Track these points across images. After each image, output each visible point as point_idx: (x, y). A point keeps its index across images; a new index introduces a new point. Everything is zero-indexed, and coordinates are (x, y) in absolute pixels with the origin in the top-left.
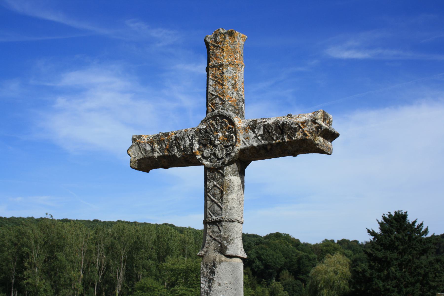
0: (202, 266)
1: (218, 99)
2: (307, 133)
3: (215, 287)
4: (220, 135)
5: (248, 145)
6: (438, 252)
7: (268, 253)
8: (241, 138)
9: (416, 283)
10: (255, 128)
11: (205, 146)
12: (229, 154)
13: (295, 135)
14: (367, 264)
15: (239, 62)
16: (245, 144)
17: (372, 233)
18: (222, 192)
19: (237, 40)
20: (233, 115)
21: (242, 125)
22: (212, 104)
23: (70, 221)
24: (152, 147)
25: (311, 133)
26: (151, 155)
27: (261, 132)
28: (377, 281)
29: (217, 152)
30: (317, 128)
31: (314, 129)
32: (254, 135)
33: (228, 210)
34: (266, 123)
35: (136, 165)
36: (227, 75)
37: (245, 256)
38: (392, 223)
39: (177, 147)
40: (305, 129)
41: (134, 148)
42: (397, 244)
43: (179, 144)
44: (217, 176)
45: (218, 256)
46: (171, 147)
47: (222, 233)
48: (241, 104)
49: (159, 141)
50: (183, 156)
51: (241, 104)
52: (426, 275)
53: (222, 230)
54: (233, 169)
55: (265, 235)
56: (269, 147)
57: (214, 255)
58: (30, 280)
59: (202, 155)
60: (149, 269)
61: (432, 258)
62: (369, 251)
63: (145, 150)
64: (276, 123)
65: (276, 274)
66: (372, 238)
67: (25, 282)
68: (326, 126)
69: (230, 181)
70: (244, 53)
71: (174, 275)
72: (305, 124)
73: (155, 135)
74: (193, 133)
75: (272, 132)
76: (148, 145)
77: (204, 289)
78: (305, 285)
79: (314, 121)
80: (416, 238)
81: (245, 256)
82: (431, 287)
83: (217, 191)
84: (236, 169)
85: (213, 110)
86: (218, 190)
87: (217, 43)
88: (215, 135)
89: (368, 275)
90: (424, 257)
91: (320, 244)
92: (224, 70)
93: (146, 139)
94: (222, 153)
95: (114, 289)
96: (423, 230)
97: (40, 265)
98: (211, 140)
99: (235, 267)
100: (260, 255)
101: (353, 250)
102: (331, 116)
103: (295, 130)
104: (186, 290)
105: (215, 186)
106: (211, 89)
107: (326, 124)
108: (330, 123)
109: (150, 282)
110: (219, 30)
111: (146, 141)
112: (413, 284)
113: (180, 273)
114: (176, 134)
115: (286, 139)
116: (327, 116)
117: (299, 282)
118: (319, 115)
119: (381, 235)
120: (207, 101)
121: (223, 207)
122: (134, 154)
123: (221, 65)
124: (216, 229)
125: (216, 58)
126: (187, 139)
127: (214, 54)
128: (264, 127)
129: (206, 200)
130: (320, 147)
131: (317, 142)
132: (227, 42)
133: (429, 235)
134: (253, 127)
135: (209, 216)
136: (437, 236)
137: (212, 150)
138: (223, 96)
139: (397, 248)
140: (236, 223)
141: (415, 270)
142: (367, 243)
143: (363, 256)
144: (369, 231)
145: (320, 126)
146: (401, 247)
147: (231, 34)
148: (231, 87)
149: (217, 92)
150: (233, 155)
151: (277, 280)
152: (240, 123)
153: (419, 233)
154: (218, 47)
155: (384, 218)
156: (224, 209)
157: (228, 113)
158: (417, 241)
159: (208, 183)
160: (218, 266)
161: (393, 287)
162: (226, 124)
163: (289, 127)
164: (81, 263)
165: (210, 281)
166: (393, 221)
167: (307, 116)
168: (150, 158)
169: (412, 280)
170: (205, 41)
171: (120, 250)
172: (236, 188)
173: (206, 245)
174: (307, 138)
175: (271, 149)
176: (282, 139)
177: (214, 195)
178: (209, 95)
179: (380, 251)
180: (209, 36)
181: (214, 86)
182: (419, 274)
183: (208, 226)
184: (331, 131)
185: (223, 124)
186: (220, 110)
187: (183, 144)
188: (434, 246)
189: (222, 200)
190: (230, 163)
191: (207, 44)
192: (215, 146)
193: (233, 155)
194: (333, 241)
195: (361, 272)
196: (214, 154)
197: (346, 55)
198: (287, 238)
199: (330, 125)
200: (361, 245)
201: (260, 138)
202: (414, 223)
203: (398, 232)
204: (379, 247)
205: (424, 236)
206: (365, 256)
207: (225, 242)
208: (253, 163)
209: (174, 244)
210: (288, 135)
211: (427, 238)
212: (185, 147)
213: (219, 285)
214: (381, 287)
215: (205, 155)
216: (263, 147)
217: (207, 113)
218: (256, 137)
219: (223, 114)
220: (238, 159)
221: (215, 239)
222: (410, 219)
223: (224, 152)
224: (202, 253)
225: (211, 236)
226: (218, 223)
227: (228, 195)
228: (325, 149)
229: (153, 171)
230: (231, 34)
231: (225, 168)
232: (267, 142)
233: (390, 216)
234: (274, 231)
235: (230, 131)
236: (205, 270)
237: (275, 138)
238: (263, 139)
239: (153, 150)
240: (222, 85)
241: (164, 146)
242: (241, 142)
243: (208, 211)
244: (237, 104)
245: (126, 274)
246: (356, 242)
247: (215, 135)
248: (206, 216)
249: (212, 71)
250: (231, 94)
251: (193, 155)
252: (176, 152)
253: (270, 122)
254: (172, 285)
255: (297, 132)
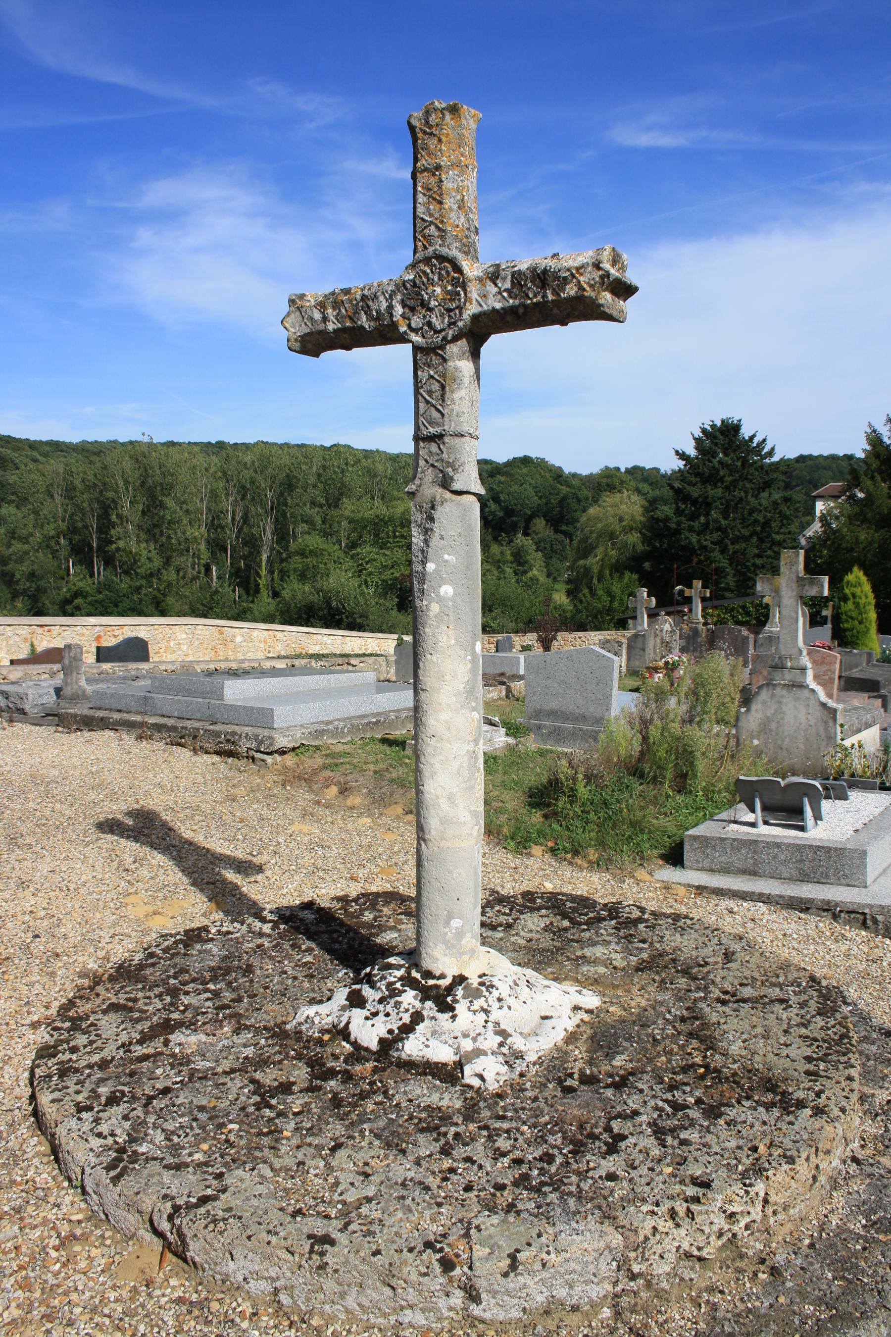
0: (413, 509)
1: (433, 228)
2: (585, 286)
3: (435, 541)
4: (438, 290)
5: (485, 308)
6: (788, 486)
7: (512, 490)
8: (474, 295)
9: (751, 536)
10: (497, 278)
11: (413, 309)
12: (454, 323)
13: (564, 290)
14: (674, 506)
15: (470, 161)
16: (481, 305)
17: (682, 456)
18: (443, 387)
19: (464, 122)
20: (459, 256)
21: (476, 273)
22: (424, 237)
23: (180, 444)
24: (323, 313)
25: (591, 286)
26: (321, 327)
27: (508, 285)
28: (687, 534)
29: (434, 320)
30: (602, 277)
31: (597, 279)
32: (496, 290)
33: (454, 417)
34: (516, 269)
35: (297, 346)
36: (448, 185)
37: (482, 491)
38: (715, 437)
39: (366, 313)
40: (581, 279)
41: (292, 316)
42: (722, 473)
43: (368, 307)
44: (435, 360)
45: (439, 492)
46: (356, 313)
47: (445, 456)
48: (473, 236)
49: (335, 302)
50: (376, 328)
51: (473, 236)
52: (766, 524)
53: (444, 450)
54: (461, 347)
55: (505, 460)
56: (521, 311)
57: (430, 490)
58: (121, 544)
59: (409, 326)
60: (309, 521)
61: (777, 496)
62: (677, 485)
63: (311, 319)
64: (533, 270)
65: (522, 524)
66: (681, 464)
67: (114, 546)
68: (617, 274)
69: (456, 369)
70: (477, 144)
71: (356, 529)
72: (582, 271)
73: (327, 292)
74: (391, 288)
75: (525, 285)
76: (315, 311)
77: (417, 544)
78: (571, 540)
79: (597, 266)
80: (755, 462)
81: (482, 491)
82: (774, 543)
83: (436, 387)
84: (467, 348)
85: (426, 248)
86: (437, 384)
87: (430, 127)
88: (429, 291)
89: (673, 526)
90: (764, 495)
91: (597, 474)
92: (444, 177)
93: (312, 301)
94: (443, 322)
95: (259, 553)
96: (766, 450)
97: (136, 517)
98: (423, 300)
99: (466, 510)
100: (498, 493)
101: (651, 484)
102: (625, 257)
103: (565, 281)
104: (377, 554)
105: (432, 377)
106: (420, 210)
107: (618, 271)
108: (623, 268)
109: (314, 541)
110: (433, 103)
111: (313, 303)
112: (745, 539)
113: (366, 526)
114: (363, 290)
115: (550, 297)
116: (619, 256)
117: (561, 537)
118: (606, 255)
119: (697, 458)
120: (415, 231)
121: (445, 412)
122: (293, 326)
123: (438, 167)
124: (434, 447)
125: (429, 155)
126: (381, 298)
127: (426, 148)
128: (513, 276)
129: (417, 402)
130: (607, 310)
131: (602, 301)
132: (447, 125)
133: (776, 458)
134: (494, 276)
135: (422, 427)
136: (789, 460)
137: (425, 316)
138: (442, 222)
139: (722, 480)
140: (468, 438)
141: (750, 514)
142: (674, 472)
143: (666, 492)
144: (677, 453)
145: (607, 275)
146: (728, 479)
147: (454, 110)
148: (455, 207)
149: (431, 215)
150: (461, 324)
151: (526, 534)
152: (472, 269)
153: (760, 455)
154: (432, 134)
155: (704, 431)
156: (446, 416)
157: (450, 253)
158: (756, 469)
159: (420, 373)
160: (439, 509)
161: (712, 543)
162: (447, 272)
163: (556, 276)
164: (202, 514)
165: (427, 531)
166: (718, 434)
167: (586, 257)
168: (320, 332)
169: (746, 532)
170: (409, 123)
171: (264, 490)
172: (466, 380)
173: (419, 475)
174: (586, 294)
175: (524, 314)
176: (543, 297)
177: (430, 393)
178: (418, 221)
179: (694, 485)
180: (416, 115)
181: (427, 205)
182: (756, 521)
183: (422, 444)
184: (625, 283)
185: (443, 272)
186: (437, 247)
187: (376, 307)
188: (783, 477)
189: (443, 401)
190: (455, 339)
191: (412, 128)
192: (430, 310)
193: (461, 324)
194: (618, 469)
195: (661, 521)
196: (429, 324)
197: (644, 140)
198: (541, 464)
199: (624, 271)
200: (664, 476)
201: (505, 294)
202: (752, 438)
203: (726, 454)
204: (693, 479)
205: (767, 461)
206: (671, 493)
207: (450, 469)
208: (493, 337)
209: (354, 478)
210: (554, 290)
211: (772, 464)
212: (378, 312)
213: (442, 538)
214: (695, 544)
215: (413, 325)
216: (512, 310)
217: (415, 253)
218: (500, 293)
219: (443, 253)
220: (470, 330)
221: (433, 465)
222: (746, 432)
223: (446, 320)
224: (412, 487)
225: (426, 461)
226: (437, 438)
227: (453, 392)
228: (615, 314)
229: (326, 355)
230: (454, 110)
231: (448, 347)
232: (517, 302)
233: (713, 426)
234: (520, 455)
235: (455, 282)
236: (418, 514)
237: (531, 295)
238: (510, 297)
239: (325, 319)
240: (440, 203)
241: (343, 311)
242: (474, 302)
243: (421, 418)
244: (467, 237)
245: (276, 529)
246: (657, 470)
247: (429, 291)
248: (417, 428)
249: (422, 179)
250: (456, 220)
251: (394, 325)
252: (364, 321)
253: (523, 266)
254: (353, 545)
255: (566, 284)
